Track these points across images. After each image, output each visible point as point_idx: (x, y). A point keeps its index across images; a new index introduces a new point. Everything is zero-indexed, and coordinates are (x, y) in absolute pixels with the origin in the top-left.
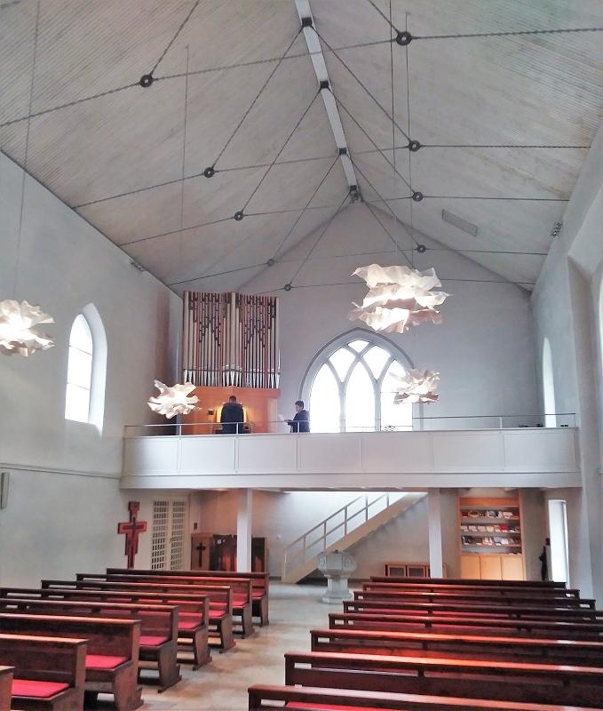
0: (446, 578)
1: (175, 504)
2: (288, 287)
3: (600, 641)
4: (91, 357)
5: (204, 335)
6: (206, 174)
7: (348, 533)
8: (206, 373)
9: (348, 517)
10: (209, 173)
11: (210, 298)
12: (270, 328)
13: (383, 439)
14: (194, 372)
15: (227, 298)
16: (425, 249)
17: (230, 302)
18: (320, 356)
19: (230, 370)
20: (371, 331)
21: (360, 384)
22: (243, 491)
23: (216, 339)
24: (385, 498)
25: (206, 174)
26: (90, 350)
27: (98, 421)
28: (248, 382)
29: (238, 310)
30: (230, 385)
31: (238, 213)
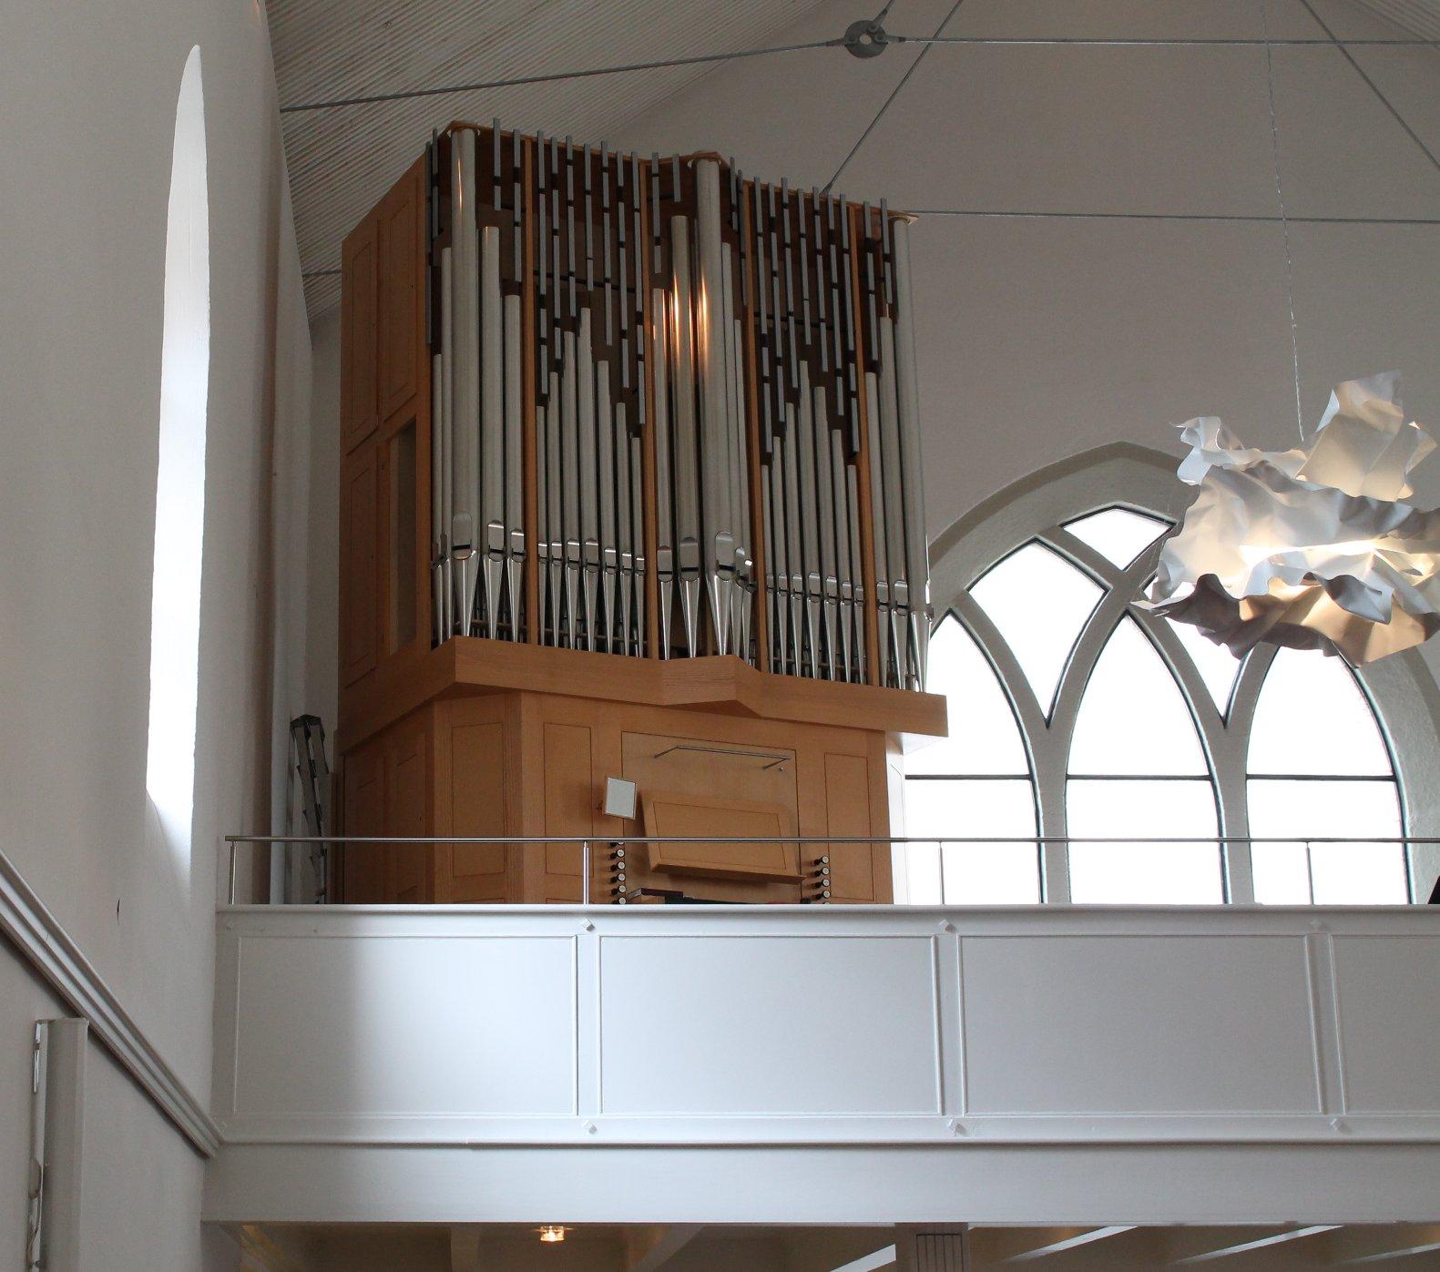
8: (572, 575)
15: (674, 185)
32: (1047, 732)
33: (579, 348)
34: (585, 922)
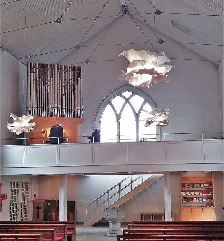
14: (34, 109)
15: (53, 66)
17: (54, 69)
18: (106, 101)
24: (141, 178)
28: (65, 114)
31: (59, 22)
32: (118, 117)
33: (42, 86)
34: (25, 146)
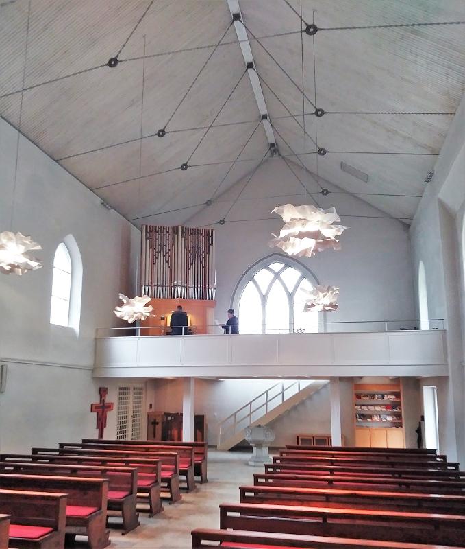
0: (344, 446)
1: (135, 389)
2: (222, 222)
3: (462, 495)
4: (70, 276)
5: (157, 258)
6: (159, 134)
7: (268, 411)
8: (158, 288)
9: (268, 400)
10: (161, 133)
11: (162, 230)
12: (209, 253)
13: (296, 339)
14: (150, 287)
15: (175, 230)
16: (327, 192)
17: (177, 233)
18: (246, 275)
19: (177, 286)
20: (286, 256)
21: (278, 297)
22: (187, 379)
23: (167, 262)
24: (297, 385)
25: (159, 134)
26: (70, 270)
27: (75, 325)
28: (192, 295)
29: (183, 239)
30: (177, 297)
31: (184, 165)
